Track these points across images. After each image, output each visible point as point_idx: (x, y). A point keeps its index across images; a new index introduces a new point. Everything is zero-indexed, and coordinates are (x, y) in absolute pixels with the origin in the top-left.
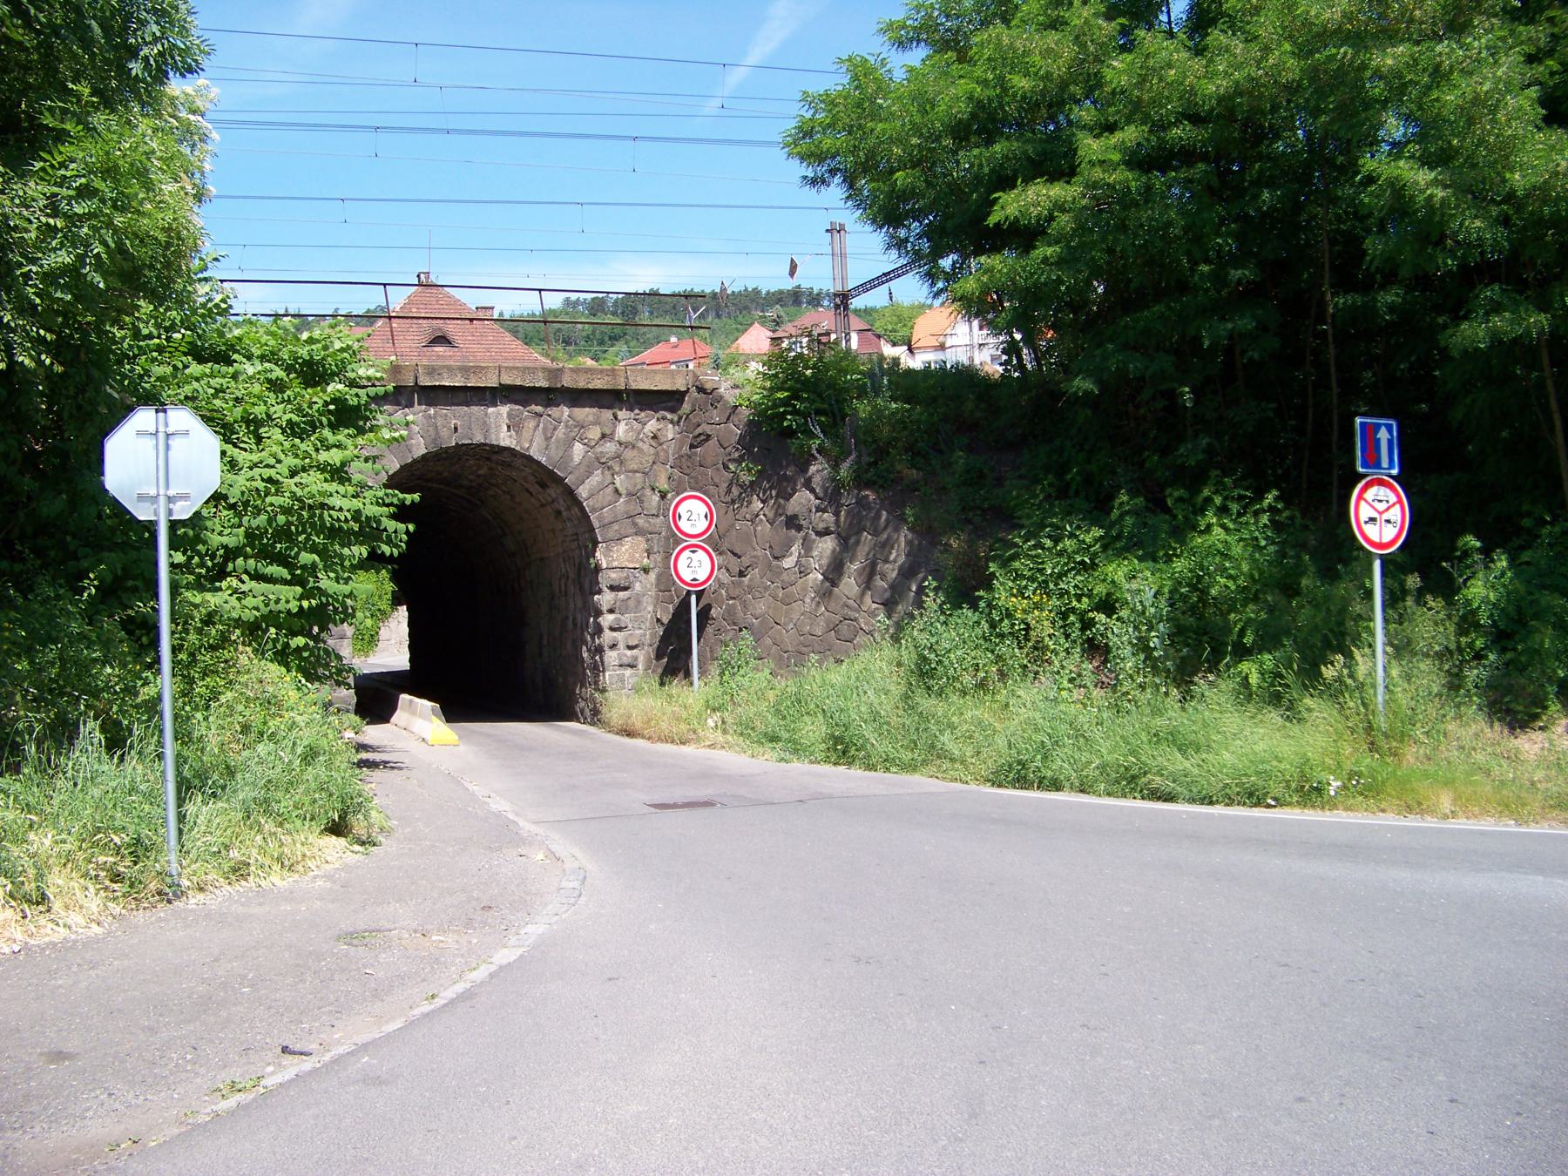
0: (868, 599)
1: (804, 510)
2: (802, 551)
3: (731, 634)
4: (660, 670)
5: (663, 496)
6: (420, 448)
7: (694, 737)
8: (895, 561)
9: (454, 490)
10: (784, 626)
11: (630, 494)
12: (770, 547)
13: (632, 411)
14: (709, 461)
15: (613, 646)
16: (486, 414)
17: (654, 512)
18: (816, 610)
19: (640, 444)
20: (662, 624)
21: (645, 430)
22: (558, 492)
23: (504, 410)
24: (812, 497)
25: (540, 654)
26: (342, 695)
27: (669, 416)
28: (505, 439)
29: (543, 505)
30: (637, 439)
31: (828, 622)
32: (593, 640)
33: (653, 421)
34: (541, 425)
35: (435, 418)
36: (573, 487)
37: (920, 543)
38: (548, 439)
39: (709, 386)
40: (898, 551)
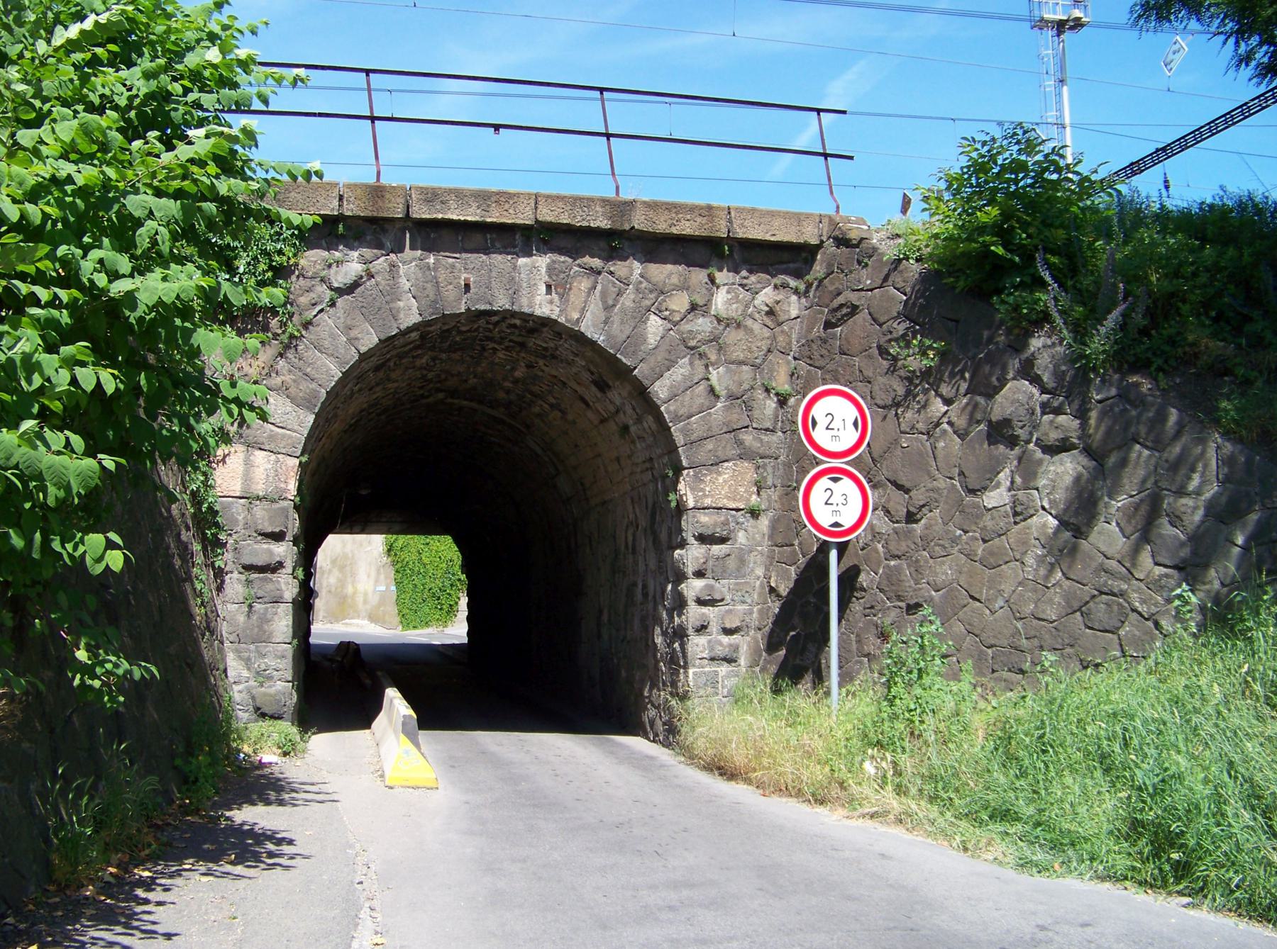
0: (1146, 558)
1: (1022, 411)
2: (1018, 480)
3: (893, 614)
4: (773, 668)
5: (782, 401)
6: (410, 314)
7: (842, 794)
8: (1198, 493)
9: (489, 411)
10: (987, 603)
11: (732, 397)
12: (961, 473)
13: (737, 272)
14: (856, 345)
15: (702, 629)
16: (515, 267)
17: (768, 425)
18: (1047, 577)
19: (749, 322)
20: (778, 596)
21: (756, 302)
22: (625, 394)
23: (542, 262)
24: (1035, 391)
25: (599, 636)
26: (272, 691)
27: (793, 283)
28: (542, 305)
29: (603, 421)
30: (744, 314)
31: (1068, 597)
32: (671, 618)
33: (769, 290)
34: (599, 287)
35: (435, 269)
36: (646, 382)
37: (1249, 461)
38: (608, 308)
39: (854, 235)
40: (1203, 475)
